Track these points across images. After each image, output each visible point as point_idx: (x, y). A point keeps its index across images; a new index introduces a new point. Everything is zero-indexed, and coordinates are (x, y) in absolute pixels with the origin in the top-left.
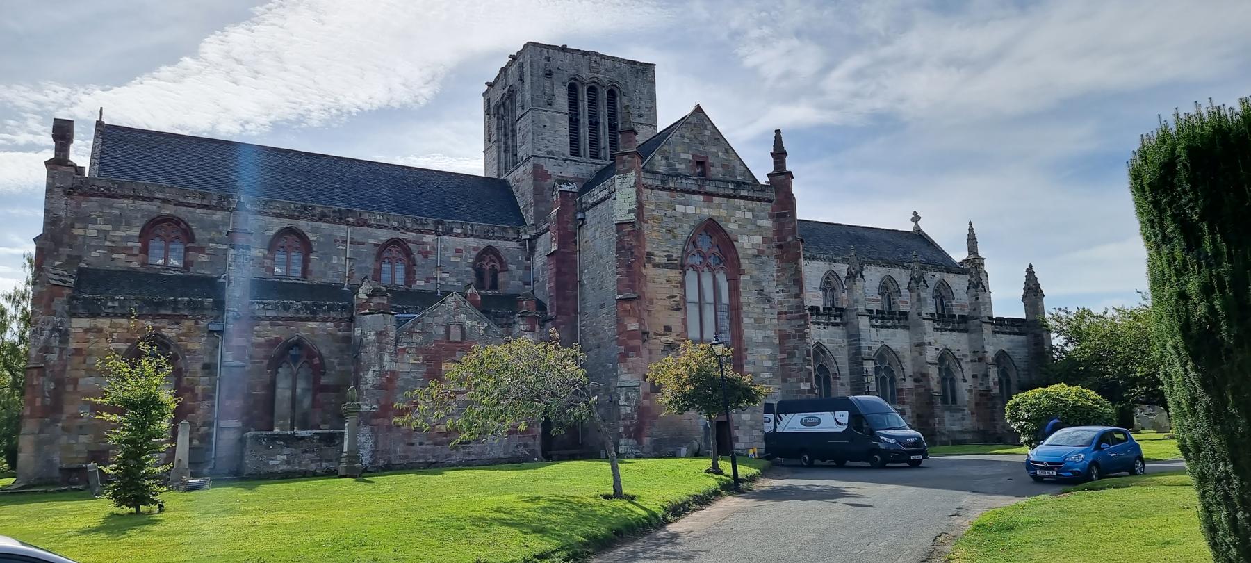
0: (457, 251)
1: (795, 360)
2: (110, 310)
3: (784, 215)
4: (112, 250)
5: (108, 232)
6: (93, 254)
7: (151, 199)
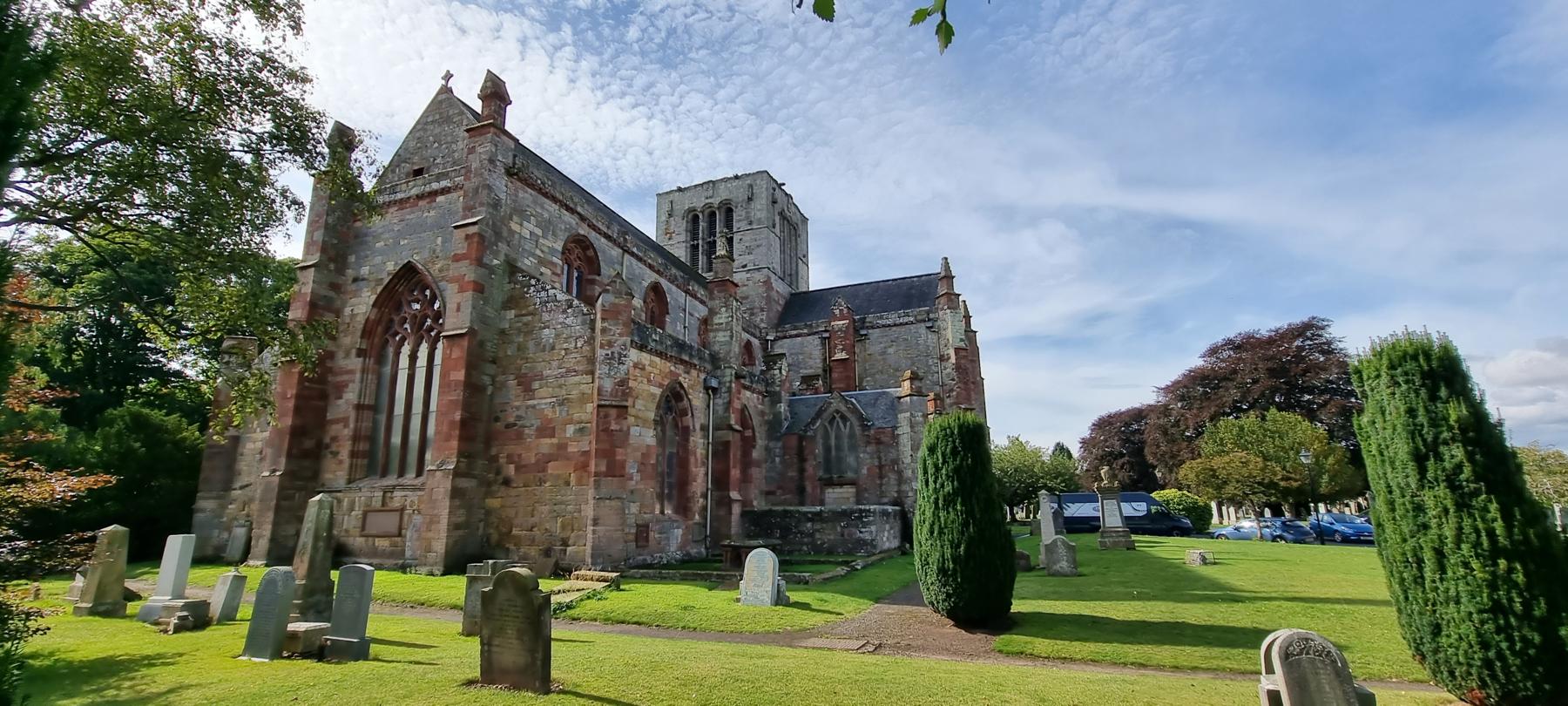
7: (572, 211)
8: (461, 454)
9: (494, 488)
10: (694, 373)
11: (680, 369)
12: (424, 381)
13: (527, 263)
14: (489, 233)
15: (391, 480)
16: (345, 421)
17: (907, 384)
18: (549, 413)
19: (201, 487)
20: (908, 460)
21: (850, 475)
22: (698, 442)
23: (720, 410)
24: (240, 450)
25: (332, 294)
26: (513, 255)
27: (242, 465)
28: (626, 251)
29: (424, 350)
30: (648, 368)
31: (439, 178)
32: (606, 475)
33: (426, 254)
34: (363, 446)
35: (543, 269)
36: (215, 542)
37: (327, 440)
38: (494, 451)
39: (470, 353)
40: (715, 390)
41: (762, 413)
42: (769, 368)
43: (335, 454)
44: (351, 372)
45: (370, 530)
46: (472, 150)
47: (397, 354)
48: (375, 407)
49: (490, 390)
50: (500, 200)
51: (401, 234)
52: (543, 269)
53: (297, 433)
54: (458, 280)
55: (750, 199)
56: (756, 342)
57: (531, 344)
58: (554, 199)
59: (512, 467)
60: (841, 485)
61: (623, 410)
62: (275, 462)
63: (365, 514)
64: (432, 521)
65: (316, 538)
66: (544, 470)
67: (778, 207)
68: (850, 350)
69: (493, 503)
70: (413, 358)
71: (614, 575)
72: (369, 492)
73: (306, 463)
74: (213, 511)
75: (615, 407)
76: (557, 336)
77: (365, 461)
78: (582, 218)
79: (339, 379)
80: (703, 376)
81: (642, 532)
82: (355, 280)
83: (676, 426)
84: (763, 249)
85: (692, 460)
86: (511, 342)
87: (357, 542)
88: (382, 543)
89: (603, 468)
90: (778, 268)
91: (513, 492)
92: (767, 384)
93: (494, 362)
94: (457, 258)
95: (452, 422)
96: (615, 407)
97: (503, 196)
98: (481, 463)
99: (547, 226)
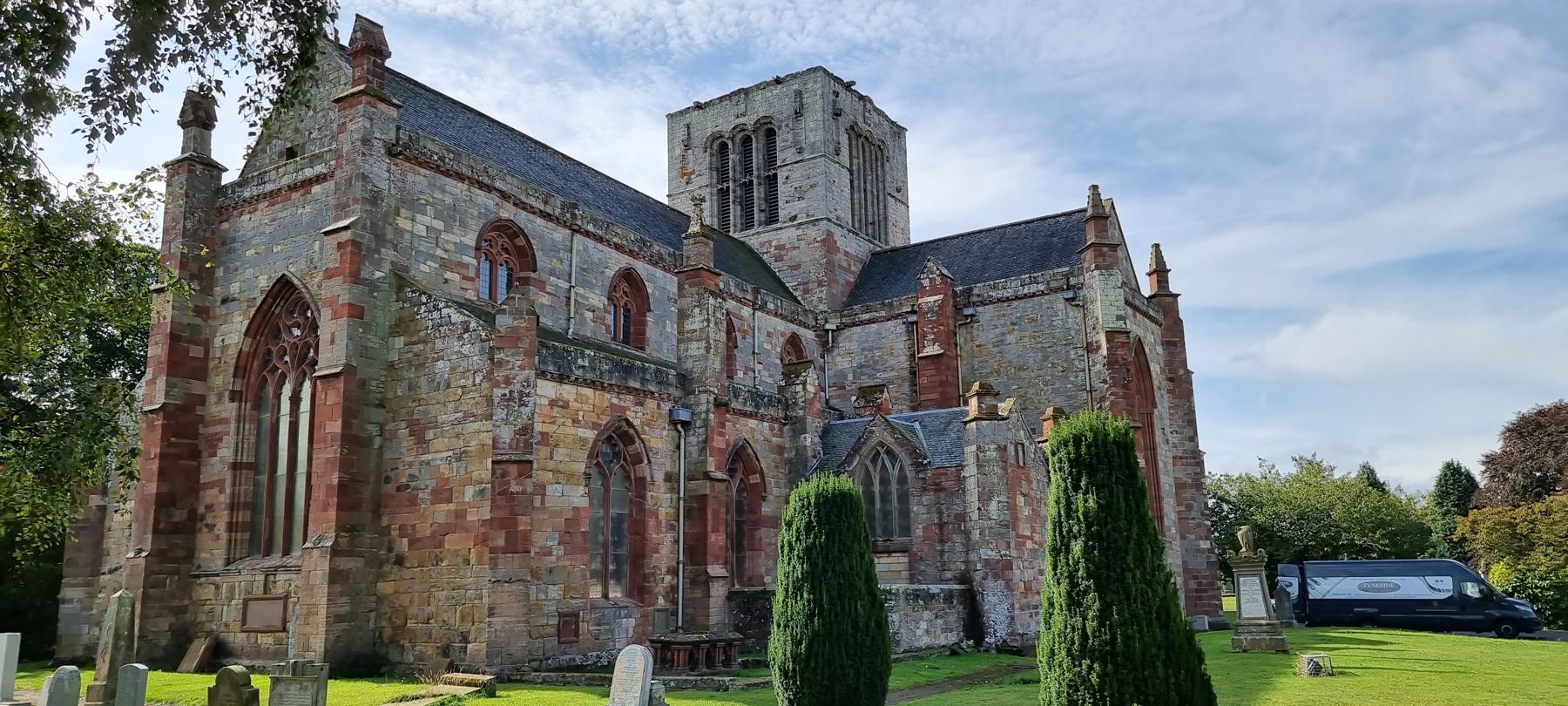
0: (769, 334)
1: (1193, 514)
2: (580, 372)
3: (1174, 344)
4: (445, 265)
5: (439, 231)
6: (423, 268)
7: (489, 188)
8: (340, 527)
9: (386, 568)
10: (651, 404)
11: (628, 401)
12: (305, 424)
13: (424, 270)
14: (367, 239)
15: (275, 560)
16: (219, 484)
17: (974, 402)
18: (444, 470)
19: (66, 571)
20: (975, 516)
21: (898, 540)
22: (661, 500)
23: (694, 450)
24: (107, 524)
25: (198, 321)
26: (403, 261)
27: (110, 543)
28: (576, 231)
29: (307, 386)
30: (574, 405)
31: (314, 159)
32: (505, 551)
33: (303, 265)
34: (243, 516)
35: (448, 275)
36: (85, 640)
37: (201, 510)
38: (385, 522)
39: (347, 398)
40: (686, 424)
41: (780, 449)
42: (790, 383)
43: (211, 527)
44: (225, 421)
45: (251, 624)
46: (342, 128)
47: (278, 396)
48: (255, 464)
49: (377, 442)
50: (380, 192)
51: (273, 239)
52: (448, 275)
53: (164, 503)
54: (331, 303)
55: (798, 114)
56: (808, 335)
57: (423, 382)
58: (460, 177)
59: (405, 541)
60: (889, 552)
61: (525, 466)
62: (140, 540)
63: (246, 603)
64: (310, 613)
65: (117, 637)
66: (441, 545)
67: (844, 122)
68: (949, 340)
69: (385, 587)
70: (295, 400)
71: (487, 678)
72: (248, 576)
73: (178, 540)
74: (80, 600)
75: (516, 463)
76: (453, 369)
77: (247, 536)
78: (504, 196)
79: (211, 430)
80: (666, 406)
81: (568, 624)
82: (224, 301)
83: (628, 478)
84: (820, 190)
85: (651, 523)
86: (401, 379)
87: (237, 639)
88: (266, 640)
89: (501, 542)
90: (846, 216)
91: (407, 574)
92: (787, 407)
93: (381, 405)
94: (329, 274)
95: (329, 486)
96: (516, 463)
97: (383, 185)
98: (367, 537)
99: (451, 215)
